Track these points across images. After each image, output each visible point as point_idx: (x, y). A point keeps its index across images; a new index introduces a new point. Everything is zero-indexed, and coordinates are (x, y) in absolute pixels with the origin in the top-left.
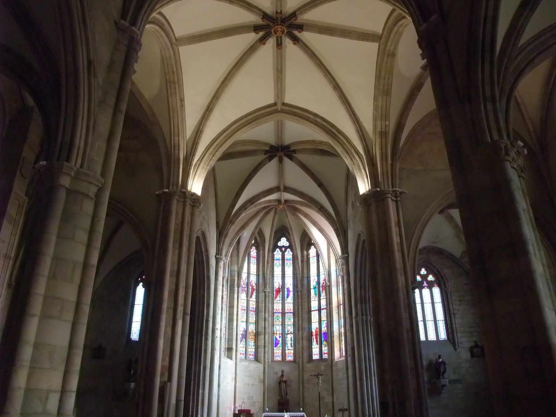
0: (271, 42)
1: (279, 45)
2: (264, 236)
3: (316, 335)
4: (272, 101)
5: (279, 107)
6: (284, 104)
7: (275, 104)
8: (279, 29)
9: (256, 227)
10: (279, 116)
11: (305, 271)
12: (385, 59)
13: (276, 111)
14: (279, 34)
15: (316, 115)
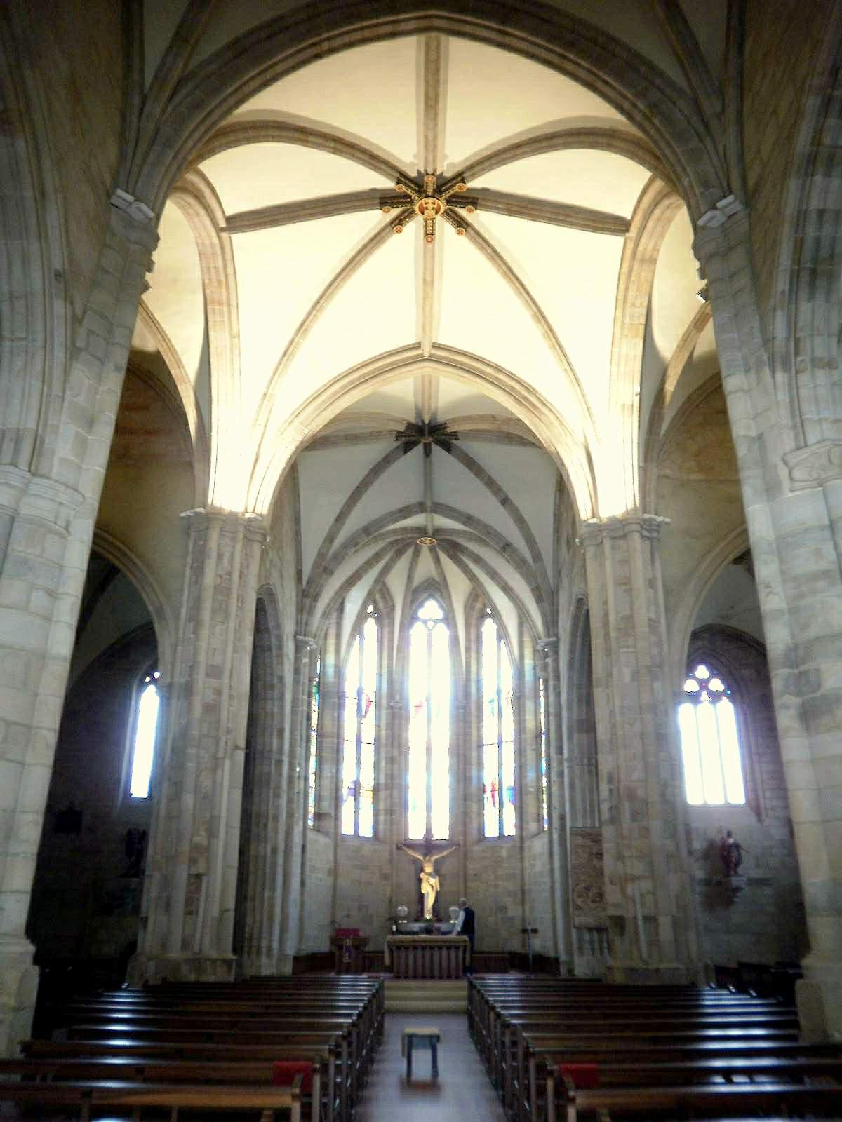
0: (413, 228)
1: (427, 452)
2: (392, 599)
3: (493, 791)
4: (412, 340)
5: (426, 351)
6: (435, 346)
7: (418, 346)
8: (430, 206)
9: (377, 581)
10: (428, 368)
11: (473, 668)
12: (636, 267)
13: (421, 359)
14: (430, 213)
15: (498, 368)
